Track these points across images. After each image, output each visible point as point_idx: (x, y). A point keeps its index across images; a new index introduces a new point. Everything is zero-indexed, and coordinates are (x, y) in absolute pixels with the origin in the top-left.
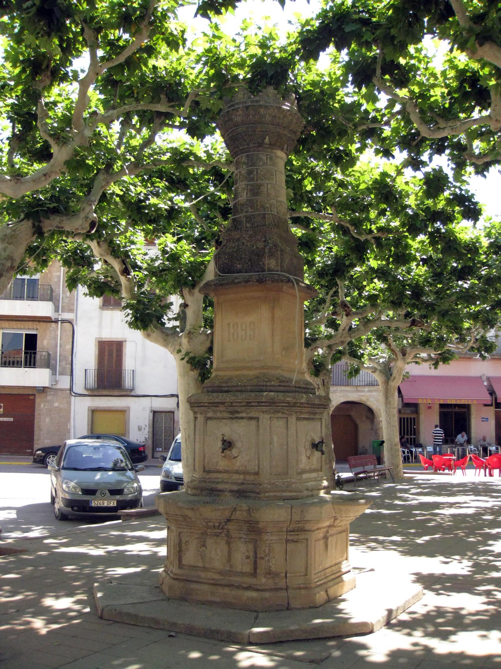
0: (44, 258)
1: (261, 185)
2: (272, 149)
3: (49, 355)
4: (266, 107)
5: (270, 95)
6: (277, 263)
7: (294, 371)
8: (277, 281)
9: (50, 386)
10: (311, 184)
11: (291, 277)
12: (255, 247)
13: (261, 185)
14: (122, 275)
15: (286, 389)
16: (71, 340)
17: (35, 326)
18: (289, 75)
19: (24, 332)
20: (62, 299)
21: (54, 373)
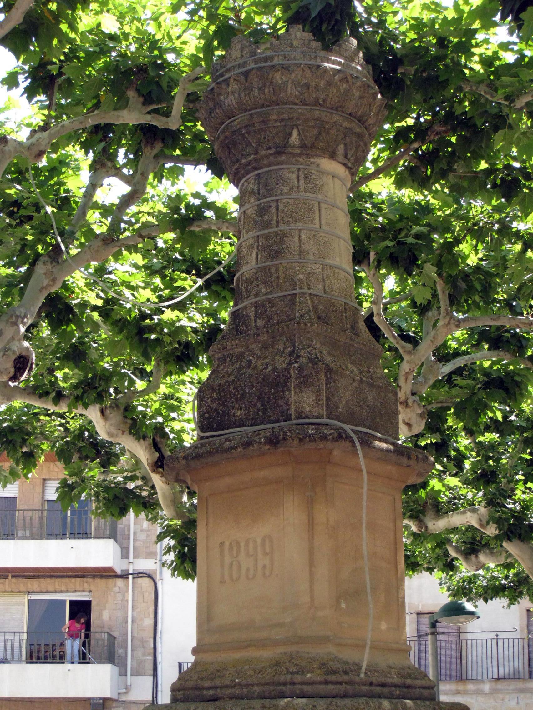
0: (25, 450)
1: (285, 235)
2: (309, 156)
3: (112, 638)
4: (285, 68)
5: (295, 44)
6: (317, 401)
7: (364, 647)
8: (312, 438)
9: (115, 697)
10: (477, 253)
11: (347, 427)
12: (270, 368)
13: (285, 235)
14: (154, 471)
15: (342, 688)
16: (152, 609)
17: (86, 586)
18: (355, 8)
19: (68, 598)
20: (135, 533)
21: (123, 673)
